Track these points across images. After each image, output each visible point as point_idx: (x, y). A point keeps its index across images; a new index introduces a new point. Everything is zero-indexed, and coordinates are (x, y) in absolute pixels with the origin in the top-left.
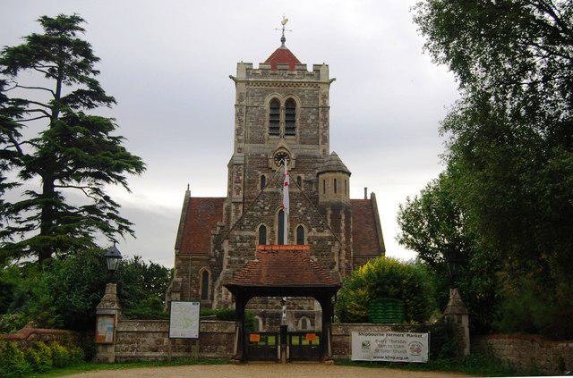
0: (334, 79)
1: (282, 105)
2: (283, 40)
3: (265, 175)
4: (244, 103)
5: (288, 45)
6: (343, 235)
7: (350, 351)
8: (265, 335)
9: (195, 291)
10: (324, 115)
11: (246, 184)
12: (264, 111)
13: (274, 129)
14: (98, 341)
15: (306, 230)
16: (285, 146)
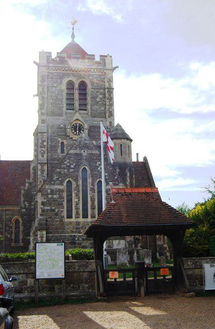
0: (117, 67)
2: (73, 36)
3: (64, 141)
4: (46, 83)
9: (9, 236)
10: (110, 95)
12: (62, 91)
13: (70, 106)
16: (80, 119)
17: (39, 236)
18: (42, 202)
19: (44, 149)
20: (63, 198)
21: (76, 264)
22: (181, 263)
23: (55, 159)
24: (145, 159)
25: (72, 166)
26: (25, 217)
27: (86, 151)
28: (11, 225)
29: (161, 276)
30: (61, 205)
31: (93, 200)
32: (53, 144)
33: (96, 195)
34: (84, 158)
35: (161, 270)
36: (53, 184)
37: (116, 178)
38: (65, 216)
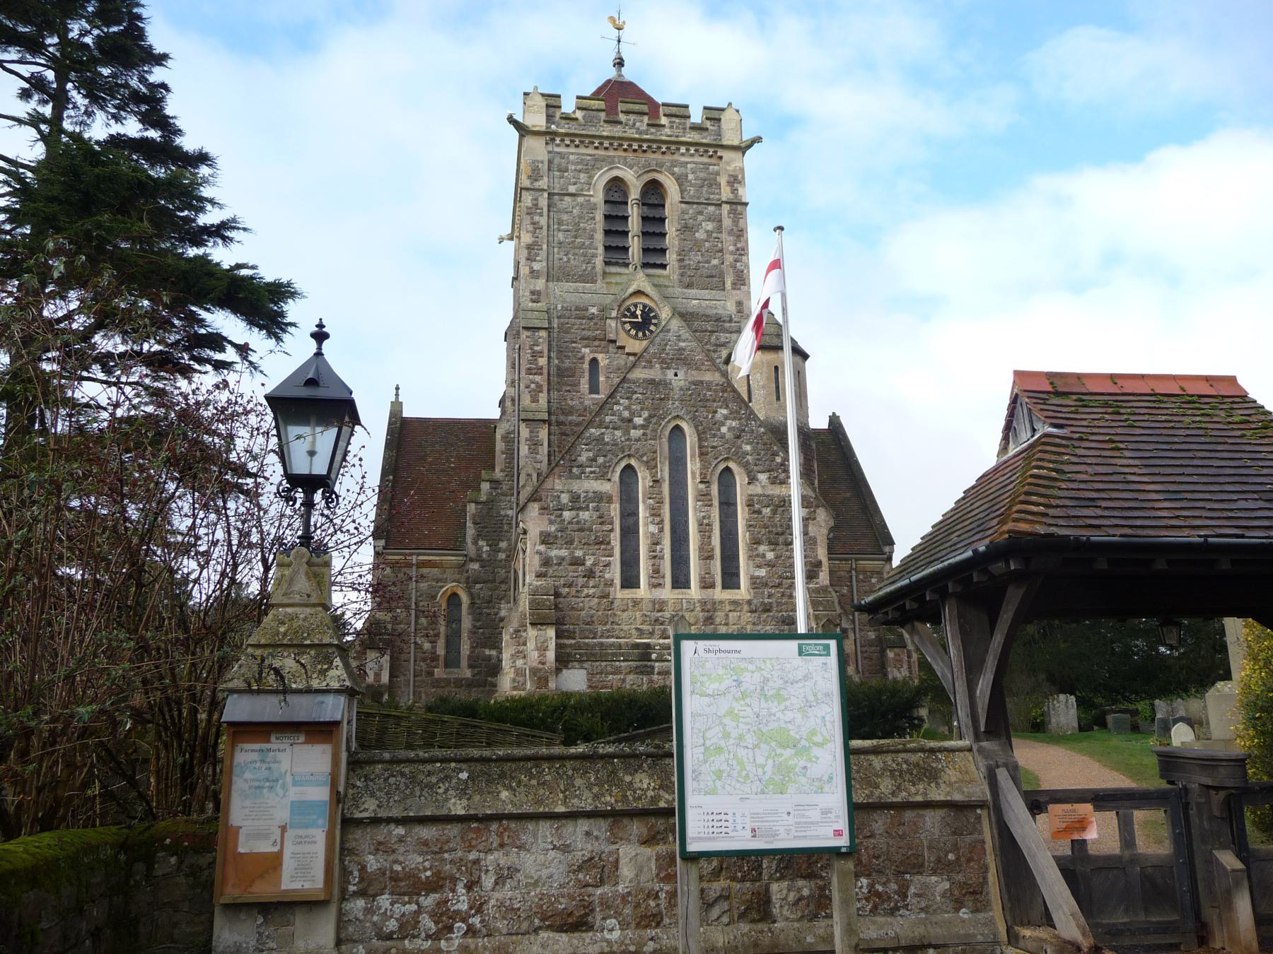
0: (758, 140)
1: (634, 194)
2: (620, 63)
3: (600, 357)
4: (543, 183)
5: (628, 74)
9: (427, 646)
10: (736, 222)
11: (554, 379)
12: (594, 207)
13: (615, 252)
14: (231, 892)
15: (740, 479)
16: (648, 289)
17: (531, 645)
18: (541, 533)
19: (538, 378)
20: (612, 523)
21: (877, 762)
23: (571, 411)
24: (835, 421)
25: (638, 421)
26: (478, 586)
27: (681, 375)
30: (603, 542)
31: (704, 528)
32: (567, 363)
33: (715, 513)
34: (677, 394)
38: (618, 582)
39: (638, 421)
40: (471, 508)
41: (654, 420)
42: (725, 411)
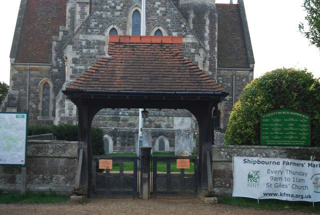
6: (207, 42)
7: (231, 186)
8: (118, 160)
9: (34, 106)
17: (66, 107)
18: (73, 59)
21: (50, 146)
22: (208, 153)
25: (118, 8)
26: (57, 80)
28: (37, 91)
29: (178, 170)
35: (178, 160)
36: (90, 34)
37: (183, 26)
39: (118, 8)
40: (54, 43)
41: (126, 8)
42: (159, 3)
